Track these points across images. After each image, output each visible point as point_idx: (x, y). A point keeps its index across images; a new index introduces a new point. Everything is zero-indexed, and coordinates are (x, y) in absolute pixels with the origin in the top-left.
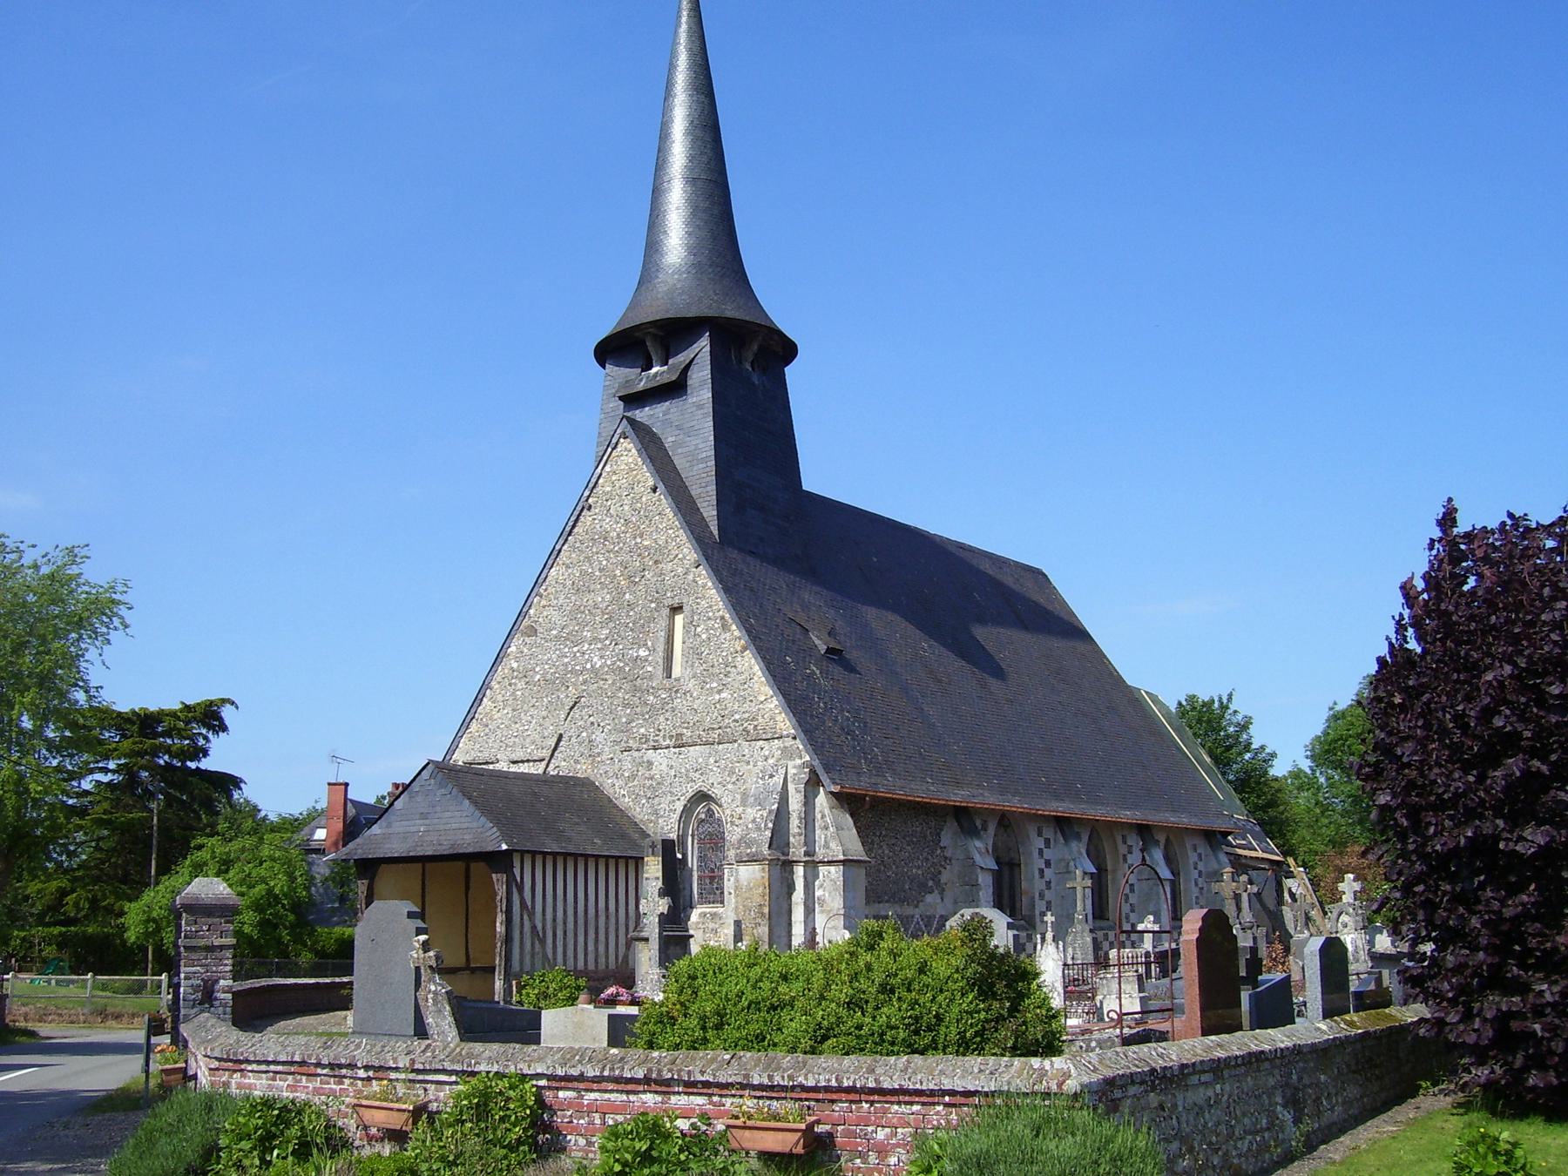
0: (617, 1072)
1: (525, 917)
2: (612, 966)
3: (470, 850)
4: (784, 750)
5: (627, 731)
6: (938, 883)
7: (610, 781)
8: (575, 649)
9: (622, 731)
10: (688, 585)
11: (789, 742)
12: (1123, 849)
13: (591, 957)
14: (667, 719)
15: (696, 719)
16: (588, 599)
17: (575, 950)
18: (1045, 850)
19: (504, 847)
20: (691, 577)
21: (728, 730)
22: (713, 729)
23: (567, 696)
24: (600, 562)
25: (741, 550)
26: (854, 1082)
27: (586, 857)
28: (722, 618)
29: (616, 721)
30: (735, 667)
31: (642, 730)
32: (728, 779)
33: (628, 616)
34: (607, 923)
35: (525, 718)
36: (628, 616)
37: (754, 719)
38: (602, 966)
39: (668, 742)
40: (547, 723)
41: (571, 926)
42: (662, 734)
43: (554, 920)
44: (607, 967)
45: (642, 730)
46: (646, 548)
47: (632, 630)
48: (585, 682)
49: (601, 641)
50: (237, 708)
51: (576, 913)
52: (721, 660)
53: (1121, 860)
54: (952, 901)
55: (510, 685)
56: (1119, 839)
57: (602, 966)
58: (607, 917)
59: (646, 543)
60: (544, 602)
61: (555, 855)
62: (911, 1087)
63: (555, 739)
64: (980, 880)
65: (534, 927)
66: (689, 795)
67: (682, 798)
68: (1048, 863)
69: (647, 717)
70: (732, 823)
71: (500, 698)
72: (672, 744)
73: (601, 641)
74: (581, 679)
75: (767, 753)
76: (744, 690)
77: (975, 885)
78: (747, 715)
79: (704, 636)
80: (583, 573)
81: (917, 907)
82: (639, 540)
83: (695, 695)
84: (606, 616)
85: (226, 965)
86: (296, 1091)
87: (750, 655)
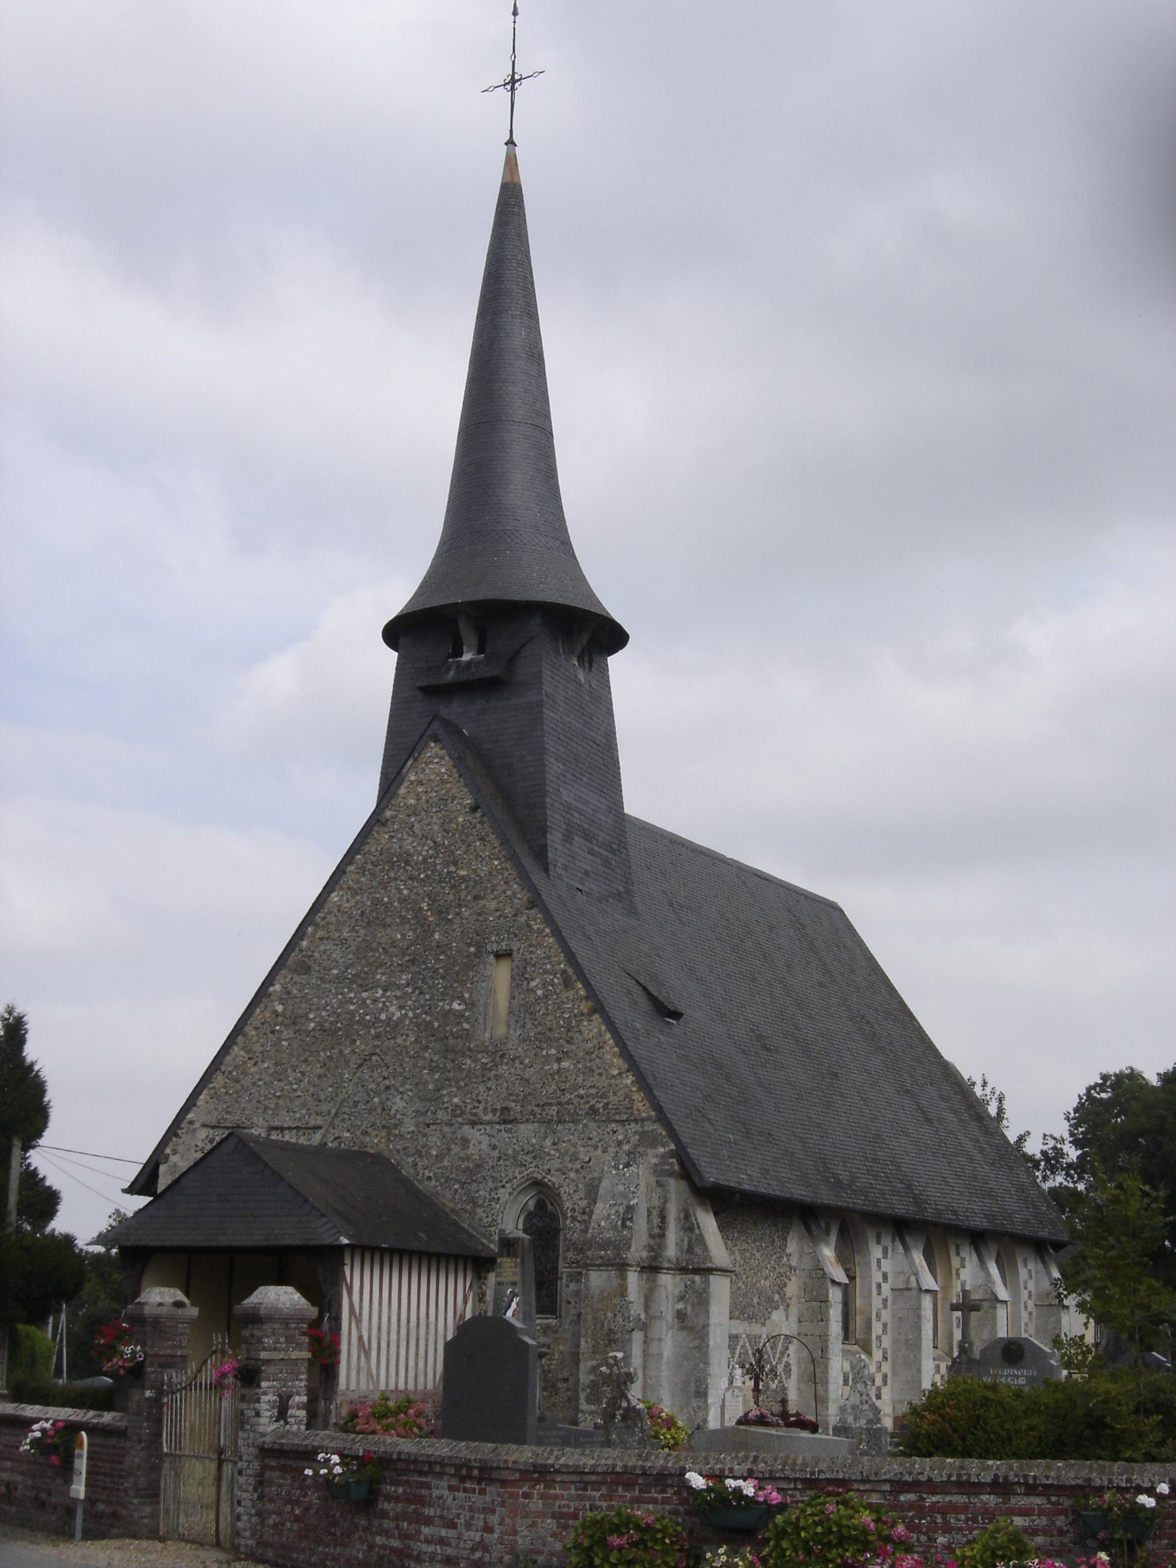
1: (354, 1325)
4: (643, 1135)
5: (436, 1100)
6: (783, 1297)
7: (410, 1160)
8: (365, 995)
9: (428, 1100)
10: (519, 928)
11: (649, 1127)
13: (411, 1374)
14: (489, 1089)
15: (527, 1091)
16: (382, 935)
17: (397, 1366)
18: (883, 1261)
20: (522, 919)
21: (571, 1107)
22: (550, 1104)
23: (353, 1052)
24: (399, 891)
28: (564, 972)
29: (420, 1087)
30: (580, 1032)
31: (456, 1100)
32: (570, 1166)
34: (427, 1334)
35: (292, 1076)
36: (438, 960)
37: (603, 1096)
38: (353, 1386)
39: (489, 1117)
41: (394, 1336)
42: (482, 1106)
43: (379, 1329)
44: (426, 1388)
45: (456, 1100)
46: (464, 879)
47: (443, 977)
48: (377, 1036)
49: (398, 987)
51: (399, 1320)
52: (562, 1023)
53: (954, 1275)
54: (796, 1319)
55: (273, 1032)
57: (421, 1387)
59: (463, 873)
60: (320, 933)
64: (831, 1296)
65: (360, 1338)
67: (508, 1185)
68: (885, 1276)
69: (462, 1084)
70: (574, 1219)
71: (257, 1048)
72: (496, 1118)
73: (398, 987)
74: (373, 1031)
75: (620, 1137)
76: (591, 1061)
77: (825, 1301)
78: (593, 1091)
79: (540, 992)
80: (377, 903)
81: (763, 1324)
82: (452, 868)
83: (527, 1061)
84: (407, 958)
85: (301, 1380)
86: (611, 1500)
87: (600, 1020)
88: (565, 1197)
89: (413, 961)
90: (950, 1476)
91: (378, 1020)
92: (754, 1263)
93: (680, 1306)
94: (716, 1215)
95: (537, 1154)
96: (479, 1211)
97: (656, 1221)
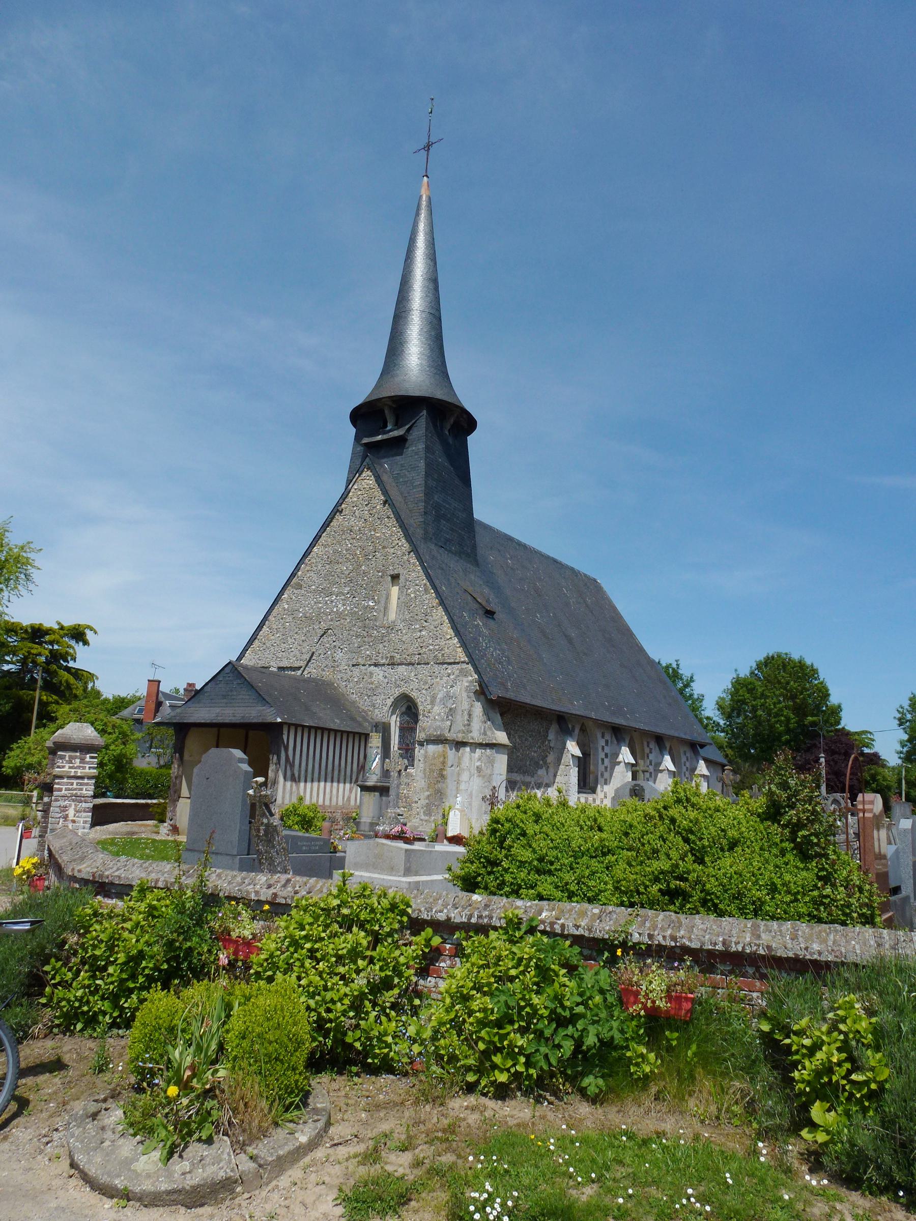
0: (485, 920)
2: (340, 803)
3: (255, 721)
4: (461, 671)
6: (545, 763)
12: (647, 750)
13: (328, 796)
19: (279, 720)
25: (436, 544)
26: (743, 948)
27: (330, 730)
28: (425, 585)
33: (363, 580)
35: (290, 641)
36: (363, 580)
40: (305, 644)
43: (306, 771)
46: (378, 538)
50: (96, 633)
51: (306, 771)
56: (645, 743)
57: (334, 803)
58: (339, 771)
60: (308, 568)
61: (310, 728)
62: (808, 957)
63: (309, 655)
66: (396, 696)
68: (606, 755)
71: (275, 627)
78: (437, 647)
88: (419, 704)
89: (351, 581)
90: (471, 916)
91: (332, 611)
92: (527, 743)
93: (478, 764)
94: (501, 715)
95: (406, 681)
96: (376, 711)
97: (466, 717)
